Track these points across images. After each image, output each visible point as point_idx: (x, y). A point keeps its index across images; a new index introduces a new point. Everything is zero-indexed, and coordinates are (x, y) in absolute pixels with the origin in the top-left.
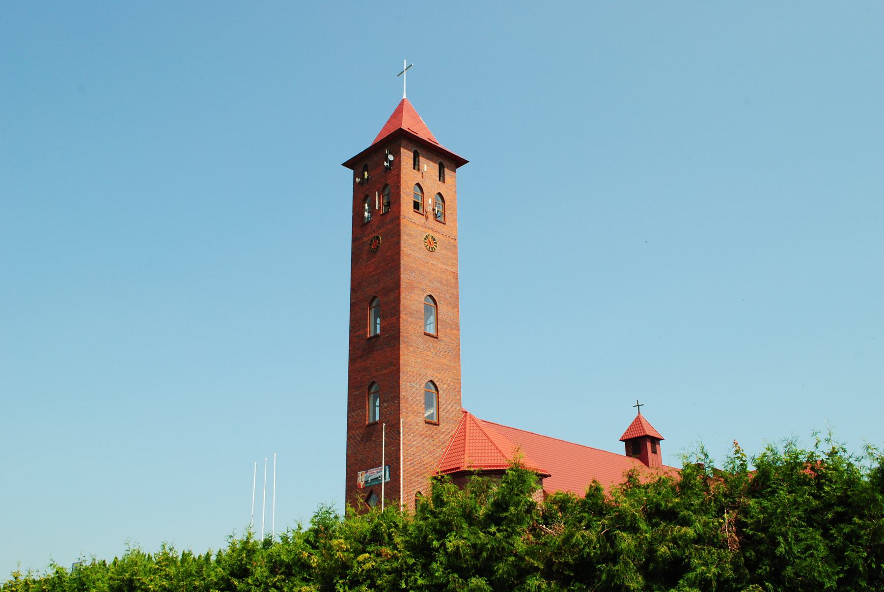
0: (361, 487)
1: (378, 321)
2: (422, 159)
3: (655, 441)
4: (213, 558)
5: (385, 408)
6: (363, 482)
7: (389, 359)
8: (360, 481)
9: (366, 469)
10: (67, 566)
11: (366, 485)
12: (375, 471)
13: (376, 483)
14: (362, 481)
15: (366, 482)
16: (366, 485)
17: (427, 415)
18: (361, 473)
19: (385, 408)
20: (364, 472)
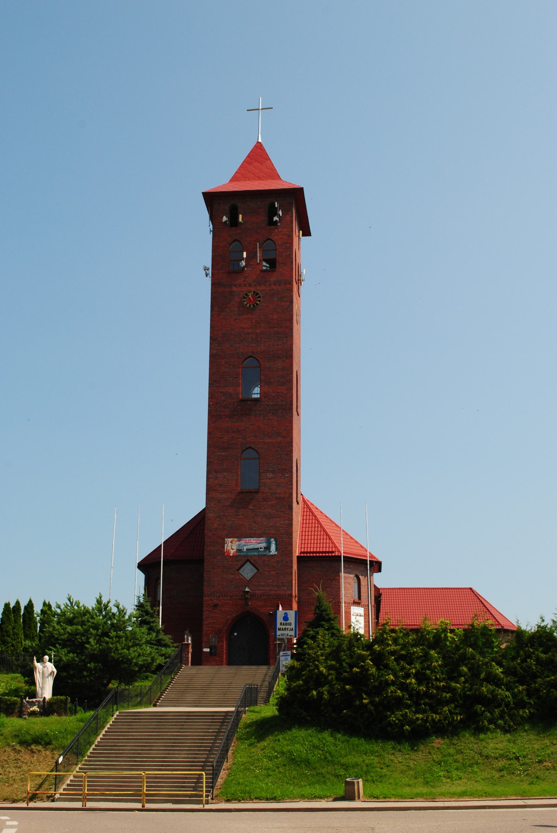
0: (231, 555)
1: (301, 232)
2: (253, 392)
3: (379, 570)
4: (38, 608)
5: (270, 479)
6: (235, 550)
7: (275, 429)
8: (229, 548)
9: (240, 537)
10: (3, 607)
11: (55, 697)
12: (254, 542)
13: (256, 554)
14: (233, 549)
15: (239, 550)
16: (238, 554)
17: (49, 683)
18: (230, 540)
19: (270, 479)
20: (236, 539)
